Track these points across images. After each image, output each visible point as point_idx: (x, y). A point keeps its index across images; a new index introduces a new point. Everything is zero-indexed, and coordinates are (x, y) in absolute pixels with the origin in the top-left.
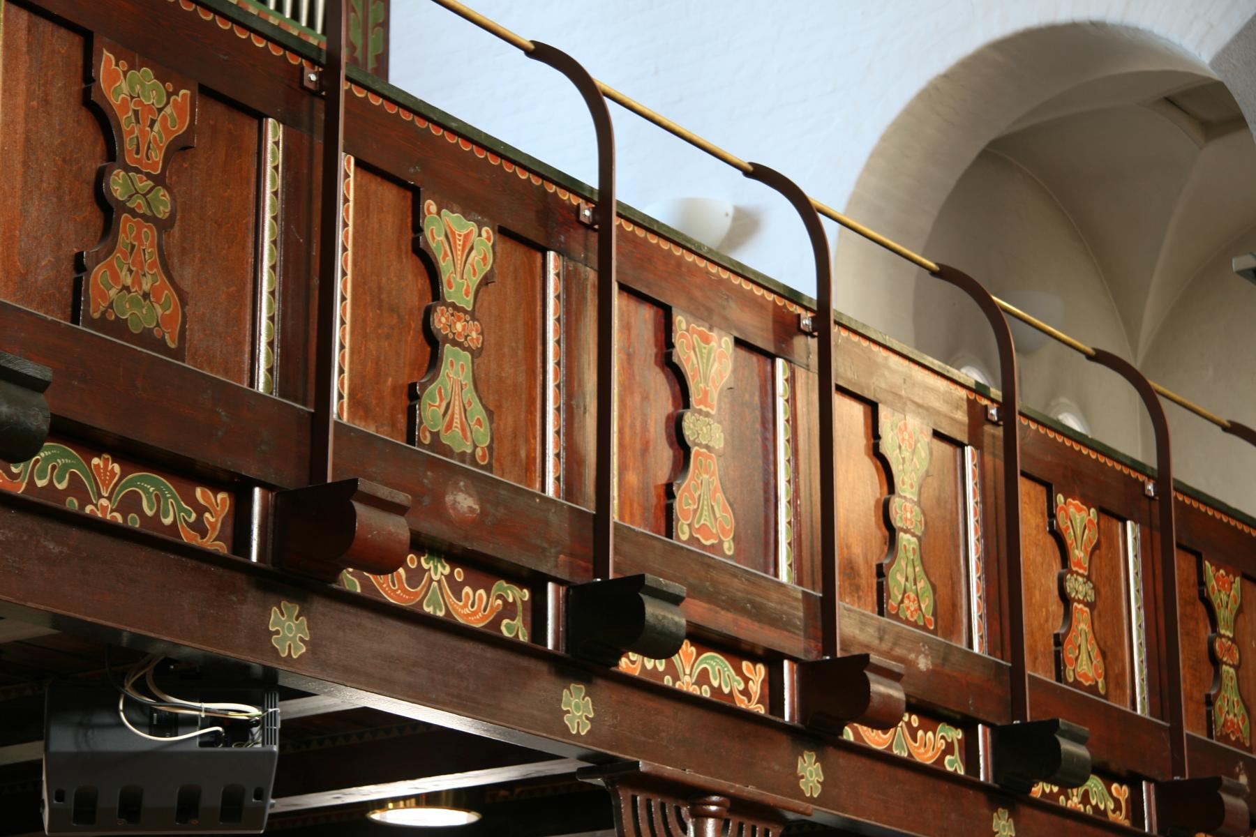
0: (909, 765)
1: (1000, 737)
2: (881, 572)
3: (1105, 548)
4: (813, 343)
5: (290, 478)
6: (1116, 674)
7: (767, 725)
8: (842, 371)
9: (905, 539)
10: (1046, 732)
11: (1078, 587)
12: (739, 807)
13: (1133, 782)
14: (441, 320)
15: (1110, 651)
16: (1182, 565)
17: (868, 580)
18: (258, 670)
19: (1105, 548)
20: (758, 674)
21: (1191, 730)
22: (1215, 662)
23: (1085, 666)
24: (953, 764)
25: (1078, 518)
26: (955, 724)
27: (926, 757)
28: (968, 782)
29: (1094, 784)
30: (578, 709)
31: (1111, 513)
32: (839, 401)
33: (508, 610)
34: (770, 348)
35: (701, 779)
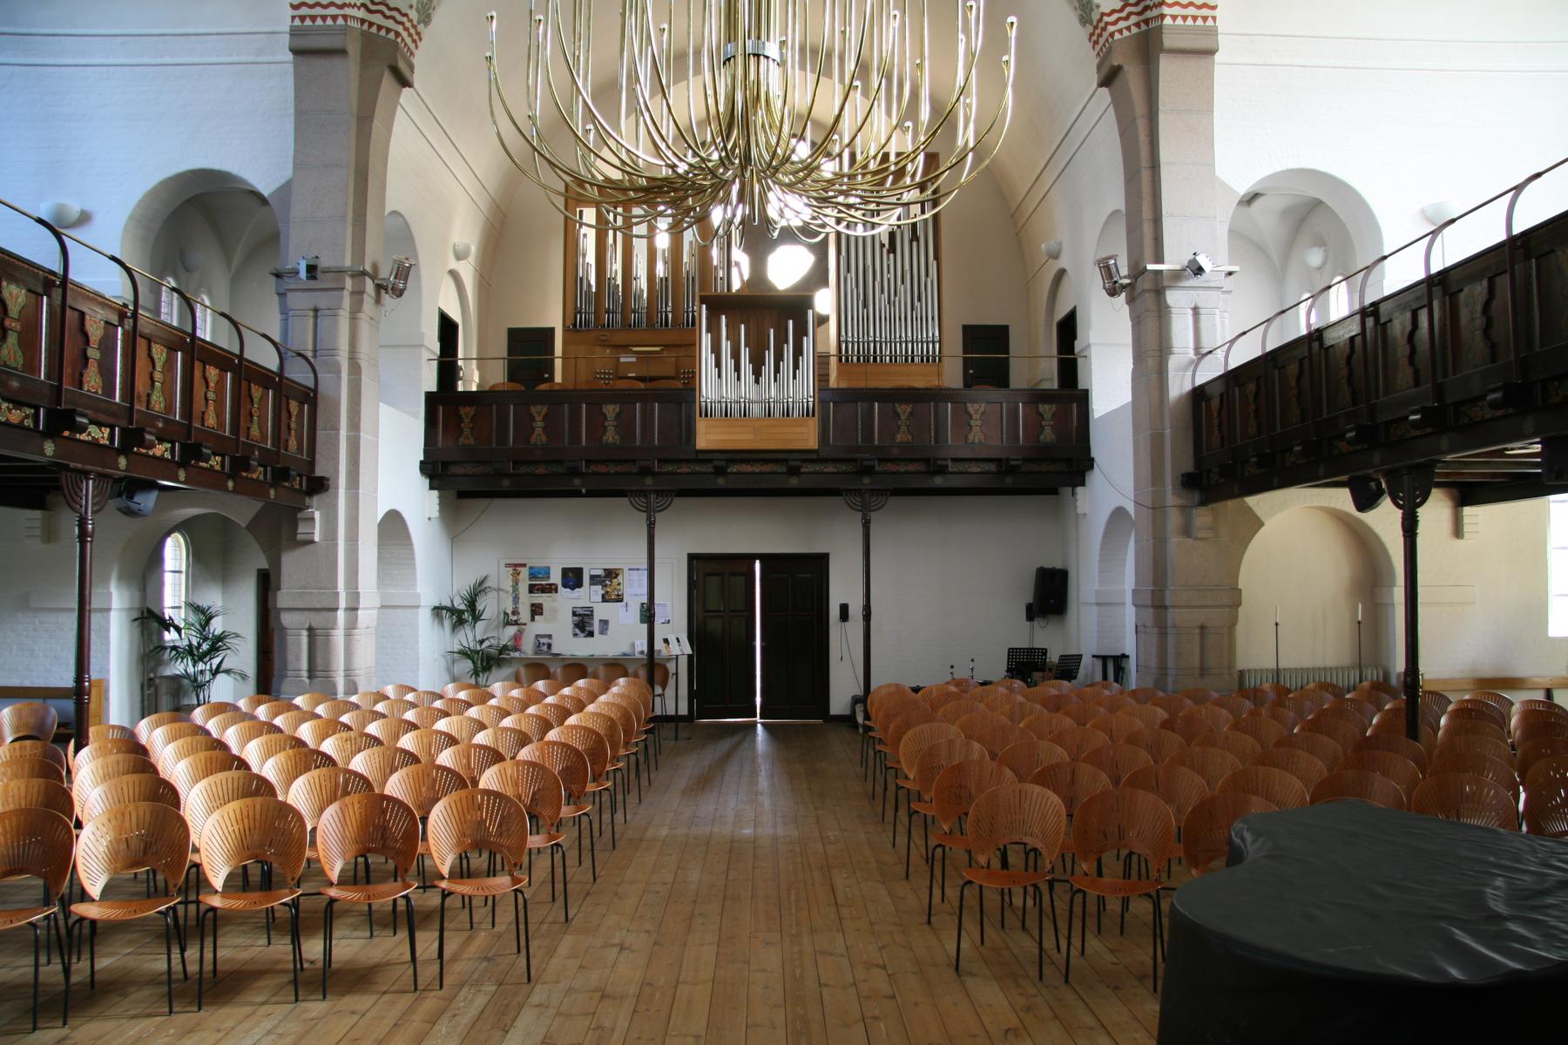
0: (154, 457)
1: (183, 447)
2: (149, 396)
3: (170, 364)
4: (60, 291)
5: (124, 423)
6: (221, 424)
7: (110, 447)
8: (70, 301)
9: (157, 384)
10: (71, 414)
11: (211, 395)
12: (100, 476)
13: (223, 456)
14: (7, 323)
15: (262, 428)
16: (244, 384)
17: (144, 399)
18: (1053, 657)
19: (170, 364)
20: (107, 431)
21: (197, 425)
22: (252, 416)
23: (211, 421)
24: (29, 423)
25: (212, 372)
26: (30, 406)
27: (158, 454)
28: (172, 461)
29: (93, 429)
30: (49, 448)
31: (223, 370)
32: (68, 311)
33: (27, 417)
34: (40, 290)
35: (88, 467)
